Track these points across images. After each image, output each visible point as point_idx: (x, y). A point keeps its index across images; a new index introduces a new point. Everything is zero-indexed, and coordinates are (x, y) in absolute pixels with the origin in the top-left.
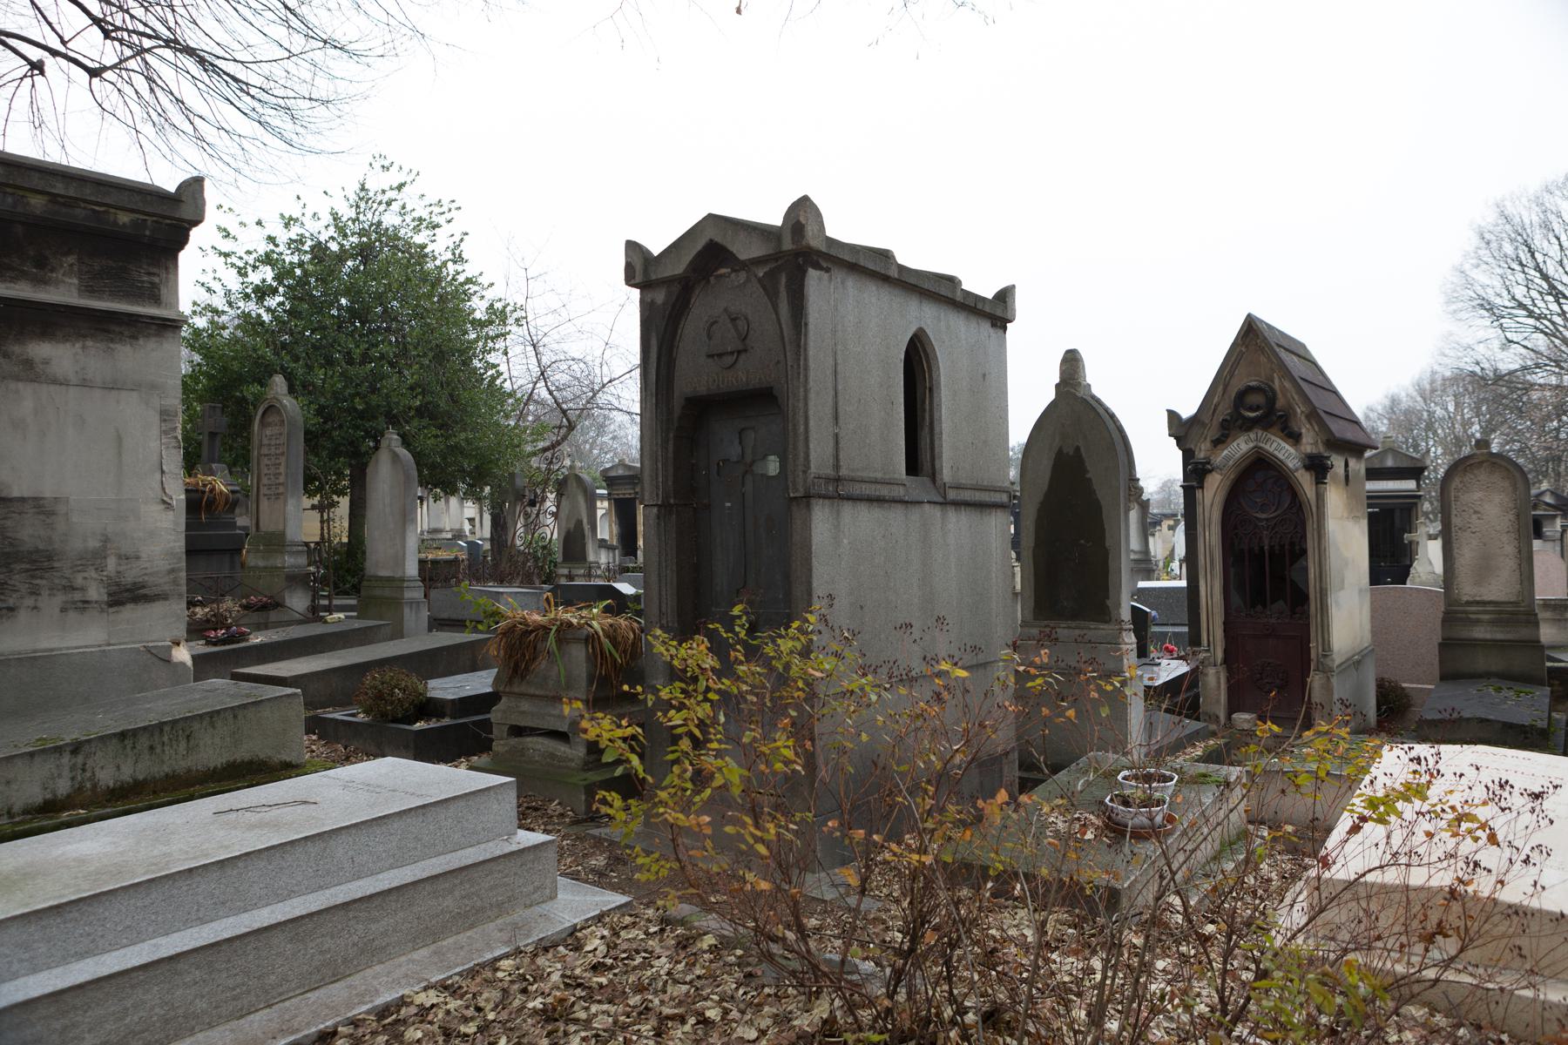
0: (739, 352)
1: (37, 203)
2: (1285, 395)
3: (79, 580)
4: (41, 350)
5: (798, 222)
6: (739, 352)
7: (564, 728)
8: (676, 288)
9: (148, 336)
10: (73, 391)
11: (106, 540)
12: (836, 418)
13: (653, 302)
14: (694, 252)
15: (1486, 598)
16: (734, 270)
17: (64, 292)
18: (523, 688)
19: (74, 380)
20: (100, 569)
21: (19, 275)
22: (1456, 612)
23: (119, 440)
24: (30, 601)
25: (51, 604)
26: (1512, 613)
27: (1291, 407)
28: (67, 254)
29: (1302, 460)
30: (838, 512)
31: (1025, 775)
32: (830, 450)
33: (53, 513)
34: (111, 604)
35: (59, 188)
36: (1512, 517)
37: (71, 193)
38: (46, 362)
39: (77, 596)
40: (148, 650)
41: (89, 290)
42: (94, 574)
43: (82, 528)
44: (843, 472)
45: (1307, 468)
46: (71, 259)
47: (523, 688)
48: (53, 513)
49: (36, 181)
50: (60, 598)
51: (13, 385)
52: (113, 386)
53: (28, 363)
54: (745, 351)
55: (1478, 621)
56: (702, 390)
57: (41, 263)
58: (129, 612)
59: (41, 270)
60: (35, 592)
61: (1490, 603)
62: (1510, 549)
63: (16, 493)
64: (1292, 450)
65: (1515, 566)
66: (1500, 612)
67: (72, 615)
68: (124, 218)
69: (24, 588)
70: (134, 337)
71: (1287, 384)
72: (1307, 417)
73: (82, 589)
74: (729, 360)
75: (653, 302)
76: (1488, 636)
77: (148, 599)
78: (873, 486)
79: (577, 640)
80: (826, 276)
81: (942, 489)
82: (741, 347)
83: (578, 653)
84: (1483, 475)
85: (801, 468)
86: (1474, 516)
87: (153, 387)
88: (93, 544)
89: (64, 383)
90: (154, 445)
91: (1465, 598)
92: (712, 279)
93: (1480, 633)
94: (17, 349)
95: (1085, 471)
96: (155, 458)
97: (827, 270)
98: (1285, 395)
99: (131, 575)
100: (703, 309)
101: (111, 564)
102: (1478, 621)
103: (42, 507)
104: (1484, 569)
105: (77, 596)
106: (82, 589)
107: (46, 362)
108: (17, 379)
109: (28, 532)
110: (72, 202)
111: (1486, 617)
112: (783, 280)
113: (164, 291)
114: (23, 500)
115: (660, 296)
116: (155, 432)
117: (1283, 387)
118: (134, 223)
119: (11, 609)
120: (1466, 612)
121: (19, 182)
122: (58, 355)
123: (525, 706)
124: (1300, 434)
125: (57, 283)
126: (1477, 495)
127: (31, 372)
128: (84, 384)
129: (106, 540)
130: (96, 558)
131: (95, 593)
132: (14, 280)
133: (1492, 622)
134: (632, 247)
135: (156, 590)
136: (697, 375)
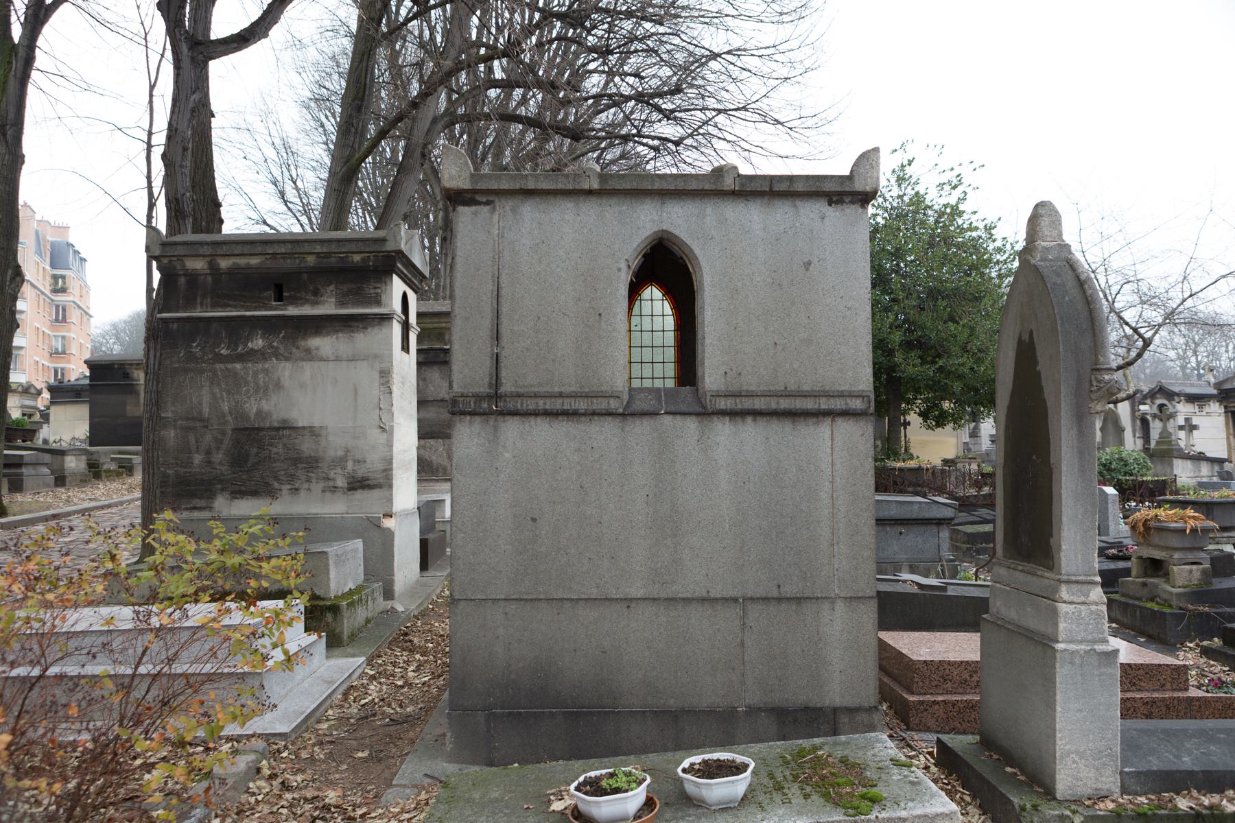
1: (311, 260)
3: (332, 475)
4: (315, 342)
9: (373, 326)
10: (331, 364)
11: (347, 451)
12: (497, 337)
17: (328, 307)
20: (343, 468)
21: (306, 301)
23: (356, 391)
24: (306, 486)
25: (317, 487)
28: (330, 284)
30: (496, 428)
32: (486, 365)
33: (319, 435)
34: (350, 489)
35: (318, 249)
37: (325, 250)
38: (317, 349)
39: (331, 484)
40: (368, 518)
41: (341, 304)
42: (340, 471)
43: (334, 445)
44: (502, 390)
46: (332, 288)
48: (319, 435)
49: (307, 248)
50: (321, 485)
51: (300, 364)
52: (353, 359)
53: (308, 351)
57: (316, 293)
58: (359, 494)
59: (316, 300)
60: (309, 481)
63: (300, 425)
67: (328, 494)
68: (357, 258)
69: (303, 478)
70: (365, 328)
73: (334, 480)
77: (370, 487)
78: (559, 401)
80: (486, 209)
81: (698, 399)
87: (376, 356)
88: (340, 453)
89: (327, 360)
90: (376, 392)
94: (303, 343)
95: (1036, 363)
96: (376, 400)
97: (487, 203)
99: (360, 473)
101: (350, 465)
103: (313, 432)
105: (331, 484)
106: (334, 480)
107: (317, 349)
108: (303, 360)
109: (306, 446)
110: (328, 255)
113: (383, 297)
114: (304, 428)
116: (377, 384)
118: (363, 259)
119: (297, 489)
121: (298, 250)
122: (323, 344)
125: (324, 303)
127: (309, 355)
128: (337, 359)
129: (347, 451)
130: (341, 461)
131: (341, 482)
132: (302, 305)
135: (375, 482)
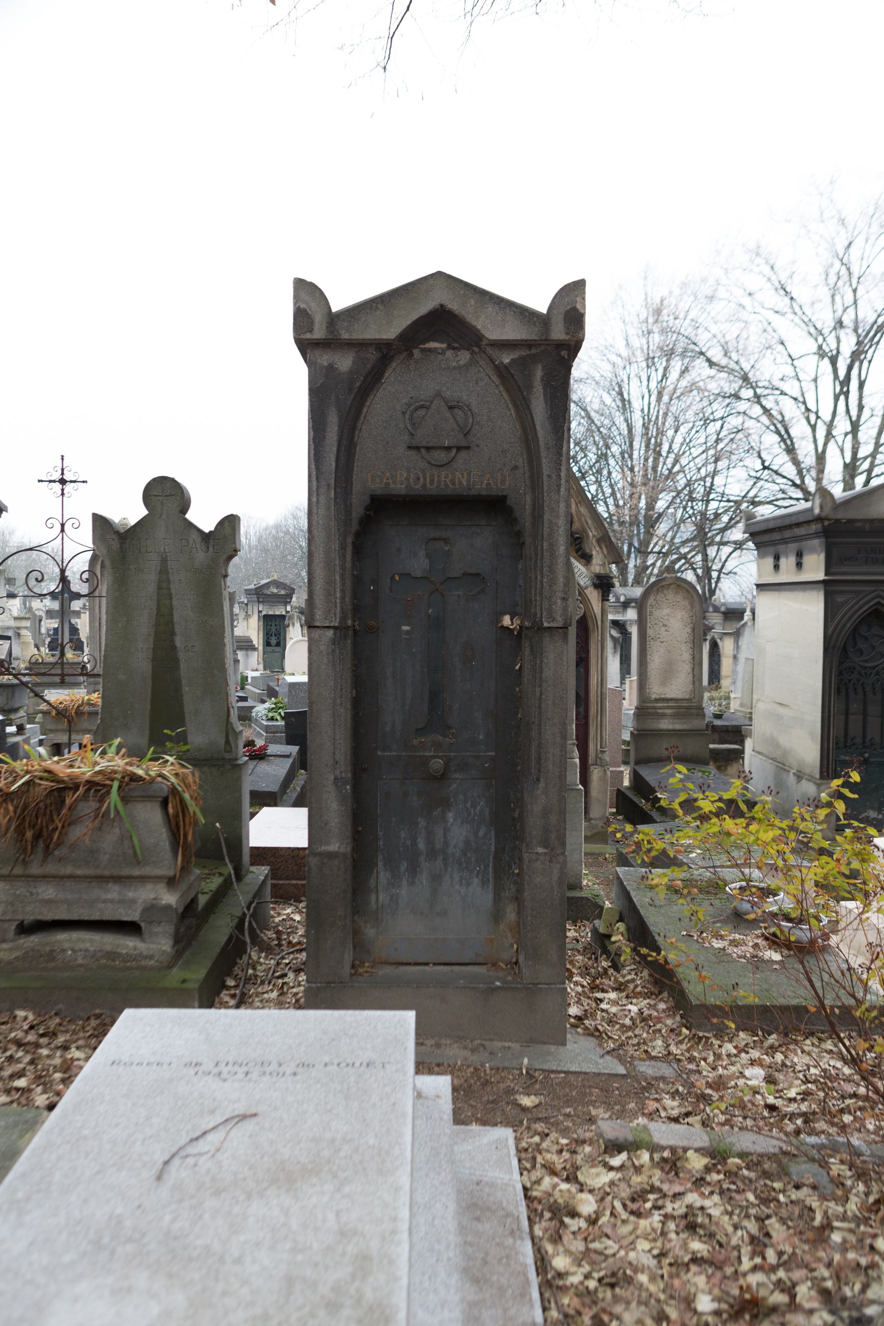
0: (459, 448)
2: (580, 520)
5: (575, 309)
6: (459, 448)
7: (133, 915)
8: (372, 356)
13: (331, 367)
14: (415, 316)
15: (669, 696)
16: (450, 347)
18: (51, 868)
19: (423, 450)
22: (648, 708)
26: (688, 708)
27: (584, 531)
29: (592, 579)
31: (275, 882)
36: (689, 630)
45: (596, 586)
47: (51, 868)
54: (468, 448)
55: (664, 715)
56: (379, 492)
61: (672, 700)
62: (687, 656)
64: (583, 569)
65: (690, 670)
66: (679, 707)
71: (583, 510)
72: (599, 541)
74: (441, 456)
75: (331, 367)
76: (670, 727)
79: (149, 798)
82: (463, 443)
83: (150, 818)
84: (670, 595)
85: (559, 595)
86: (663, 629)
91: (654, 696)
92: (416, 353)
93: (665, 724)
98: (580, 520)
100: (396, 389)
102: (664, 715)
104: (668, 672)
111: (669, 711)
112: (539, 373)
115: (344, 362)
117: (578, 512)
120: (655, 708)
123: (48, 891)
124: (591, 556)
126: (666, 611)
133: (675, 716)
134: (306, 292)
136: (391, 467)
